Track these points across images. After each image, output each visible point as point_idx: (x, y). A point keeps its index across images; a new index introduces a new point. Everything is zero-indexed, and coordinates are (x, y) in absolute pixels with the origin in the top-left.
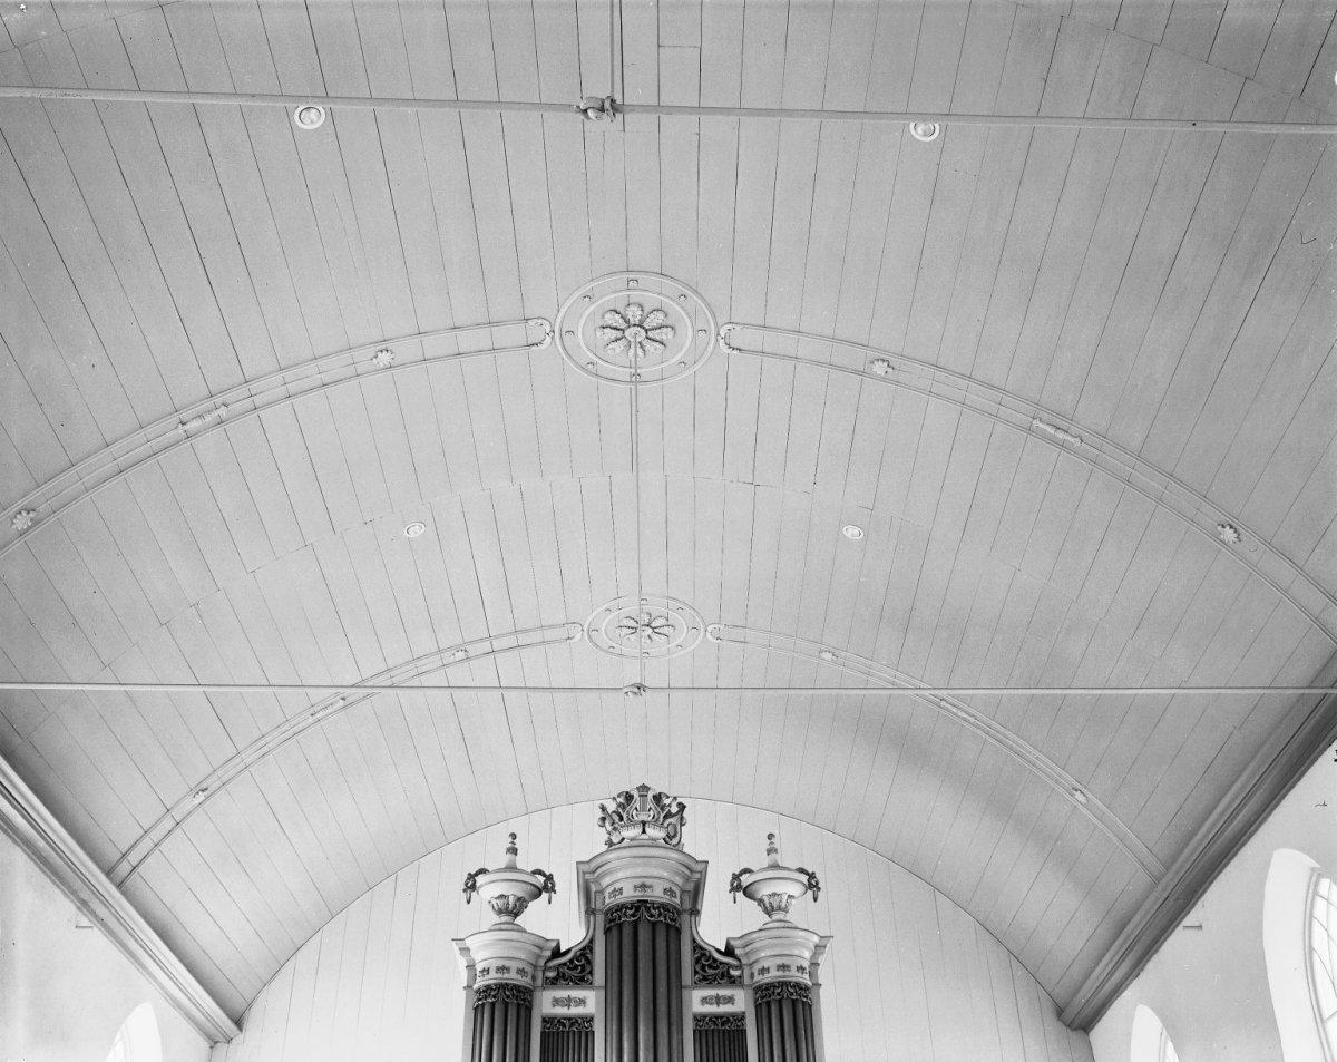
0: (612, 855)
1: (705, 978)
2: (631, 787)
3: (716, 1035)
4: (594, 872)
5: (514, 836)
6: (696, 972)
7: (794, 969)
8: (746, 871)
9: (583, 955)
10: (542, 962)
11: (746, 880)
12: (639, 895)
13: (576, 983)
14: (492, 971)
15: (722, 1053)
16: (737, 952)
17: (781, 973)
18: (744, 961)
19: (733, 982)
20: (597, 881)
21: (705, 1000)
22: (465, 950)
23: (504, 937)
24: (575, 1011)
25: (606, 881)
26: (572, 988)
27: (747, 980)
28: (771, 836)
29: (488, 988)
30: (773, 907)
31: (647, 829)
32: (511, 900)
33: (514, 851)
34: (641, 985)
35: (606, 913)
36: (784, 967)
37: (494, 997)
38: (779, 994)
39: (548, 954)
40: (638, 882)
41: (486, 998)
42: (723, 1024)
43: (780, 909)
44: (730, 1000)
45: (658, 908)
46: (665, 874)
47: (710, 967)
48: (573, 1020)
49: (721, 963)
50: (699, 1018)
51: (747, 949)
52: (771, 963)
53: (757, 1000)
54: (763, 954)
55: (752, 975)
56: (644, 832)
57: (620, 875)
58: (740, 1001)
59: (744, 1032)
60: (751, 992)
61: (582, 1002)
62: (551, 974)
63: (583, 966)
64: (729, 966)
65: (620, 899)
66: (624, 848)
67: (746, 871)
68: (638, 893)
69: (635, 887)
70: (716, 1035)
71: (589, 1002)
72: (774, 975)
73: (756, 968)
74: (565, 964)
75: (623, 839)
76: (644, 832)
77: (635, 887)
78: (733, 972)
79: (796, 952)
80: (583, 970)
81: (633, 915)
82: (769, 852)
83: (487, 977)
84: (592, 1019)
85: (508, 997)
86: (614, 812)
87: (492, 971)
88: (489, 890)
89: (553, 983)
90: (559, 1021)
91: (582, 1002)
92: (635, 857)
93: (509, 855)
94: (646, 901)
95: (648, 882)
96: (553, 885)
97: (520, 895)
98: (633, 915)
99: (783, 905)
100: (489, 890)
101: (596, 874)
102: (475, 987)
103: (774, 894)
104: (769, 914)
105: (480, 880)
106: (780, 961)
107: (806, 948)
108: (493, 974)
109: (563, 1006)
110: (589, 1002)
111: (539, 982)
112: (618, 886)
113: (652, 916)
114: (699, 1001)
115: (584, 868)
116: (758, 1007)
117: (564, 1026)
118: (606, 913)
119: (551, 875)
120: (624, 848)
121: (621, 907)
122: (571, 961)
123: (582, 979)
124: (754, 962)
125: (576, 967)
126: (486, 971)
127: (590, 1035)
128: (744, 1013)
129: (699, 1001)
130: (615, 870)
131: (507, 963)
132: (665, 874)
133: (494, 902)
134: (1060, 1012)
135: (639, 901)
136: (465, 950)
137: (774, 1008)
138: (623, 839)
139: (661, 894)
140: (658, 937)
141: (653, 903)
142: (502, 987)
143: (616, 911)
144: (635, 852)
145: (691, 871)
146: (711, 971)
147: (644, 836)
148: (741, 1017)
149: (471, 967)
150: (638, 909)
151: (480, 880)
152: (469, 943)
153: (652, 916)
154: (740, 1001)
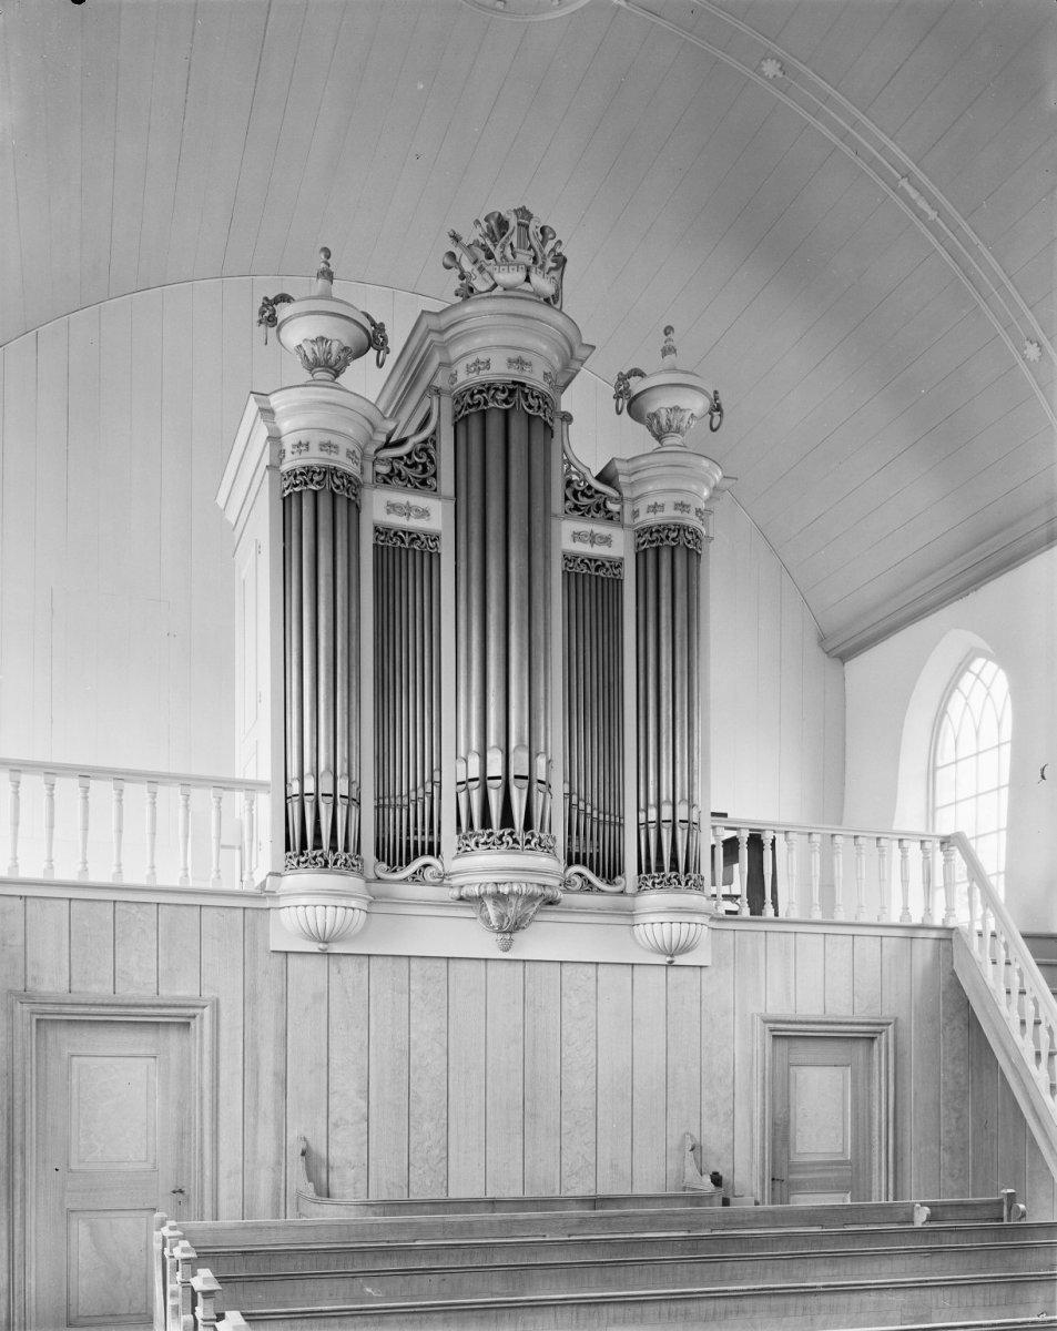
0: (469, 309)
1: (577, 508)
2: (506, 208)
3: (611, 584)
4: (441, 332)
5: (327, 252)
6: (566, 499)
7: (693, 510)
8: (637, 373)
9: (424, 450)
10: (371, 450)
11: (636, 385)
12: (514, 374)
13: (416, 487)
14: (314, 448)
15: (581, 608)
16: (622, 479)
17: (678, 513)
18: (626, 493)
19: (610, 517)
20: (444, 347)
21: (577, 536)
22: (267, 413)
23: (332, 399)
24: (598, 551)
25: (456, 351)
26: (409, 492)
27: (627, 519)
28: (668, 330)
29: (308, 471)
30: (670, 426)
31: (533, 277)
32: (335, 347)
33: (328, 275)
34: (339, 557)
35: (458, 399)
36: (682, 506)
37: (318, 483)
38: (673, 540)
39: (383, 439)
40: (514, 355)
41: (306, 484)
42: (597, 569)
43: (678, 430)
44: (607, 540)
45: (538, 397)
46: (545, 347)
47: (583, 494)
48: (414, 537)
49: (597, 492)
50: (569, 559)
51: (633, 479)
52: (668, 500)
53: (638, 545)
54: (650, 488)
55: (635, 514)
56: (528, 279)
57: (492, 339)
58: (618, 545)
59: (619, 582)
60: (630, 535)
61: (425, 513)
62: (384, 469)
63: (424, 465)
64: (608, 498)
65: (485, 376)
66: (495, 297)
67: (637, 373)
68: (513, 371)
69: (510, 361)
70: (611, 584)
71: (432, 515)
72: (668, 515)
73: (642, 506)
74: (401, 458)
75: (495, 285)
76: (528, 279)
77: (510, 361)
78: (610, 506)
79: (694, 487)
80: (425, 470)
81: (506, 401)
82: (665, 352)
83: (304, 454)
84: (436, 538)
85: (338, 487)
86: (476, 243)
87: (314, 448)
88: (299, 331)
89: (385, 482)
90: (395, 534)
91: (425, 513)
92: (515, 315)
93: (321, 281)
94: (523, 385)
95: (526, 357)
96: (385, 339)
97: (346, 343)
98: (506, 401)
99: (684, 425)
100: (299, 331)
101: (447, 335)
102: (285, 467)
103: (676, 409)
104: (659, 438)
105: (283, 311)
106: (678, 498)
107: (707, 485)
108: (315, 450)
109: (400, 514)
110: (432, 515)
111: (369, 476)
112: (482, 357)
113: (530, 407)
114: (570, 536)
115: (429, 321)
116: (640, 555)
117: (403, 542)
118: (458, 399)
119: (382, 324)
120: (495, 297)
121: (488, 388)
122: (409, 455)
123: (424, 483)
124: (638, 498)
125: (415, 465)
126: (301, 446)
127: (434, 557)
128: (623, 559)
129: (570, 536)
130: (469, 334)
131: (335, 440)
132: (351, 431)
133: (307, 348)
134: (822, 640)
135: (514, 383)
136: (267, 413)
137: (665, 556)
138: (495, 285)
139: (541, 379)
140: (534, 443)
141: (532, 390)
142: (330, 472)
143: (480, 392)
144: (506, 306)
145: (374, 429)
146: (585, 501)
147: (527, 286)
148: (618, 564)
149: (275, 439)
150: (512, 392)
151: (283, 311)
152: (275, 401)
153: (530, 407)
154: (618, 545)
